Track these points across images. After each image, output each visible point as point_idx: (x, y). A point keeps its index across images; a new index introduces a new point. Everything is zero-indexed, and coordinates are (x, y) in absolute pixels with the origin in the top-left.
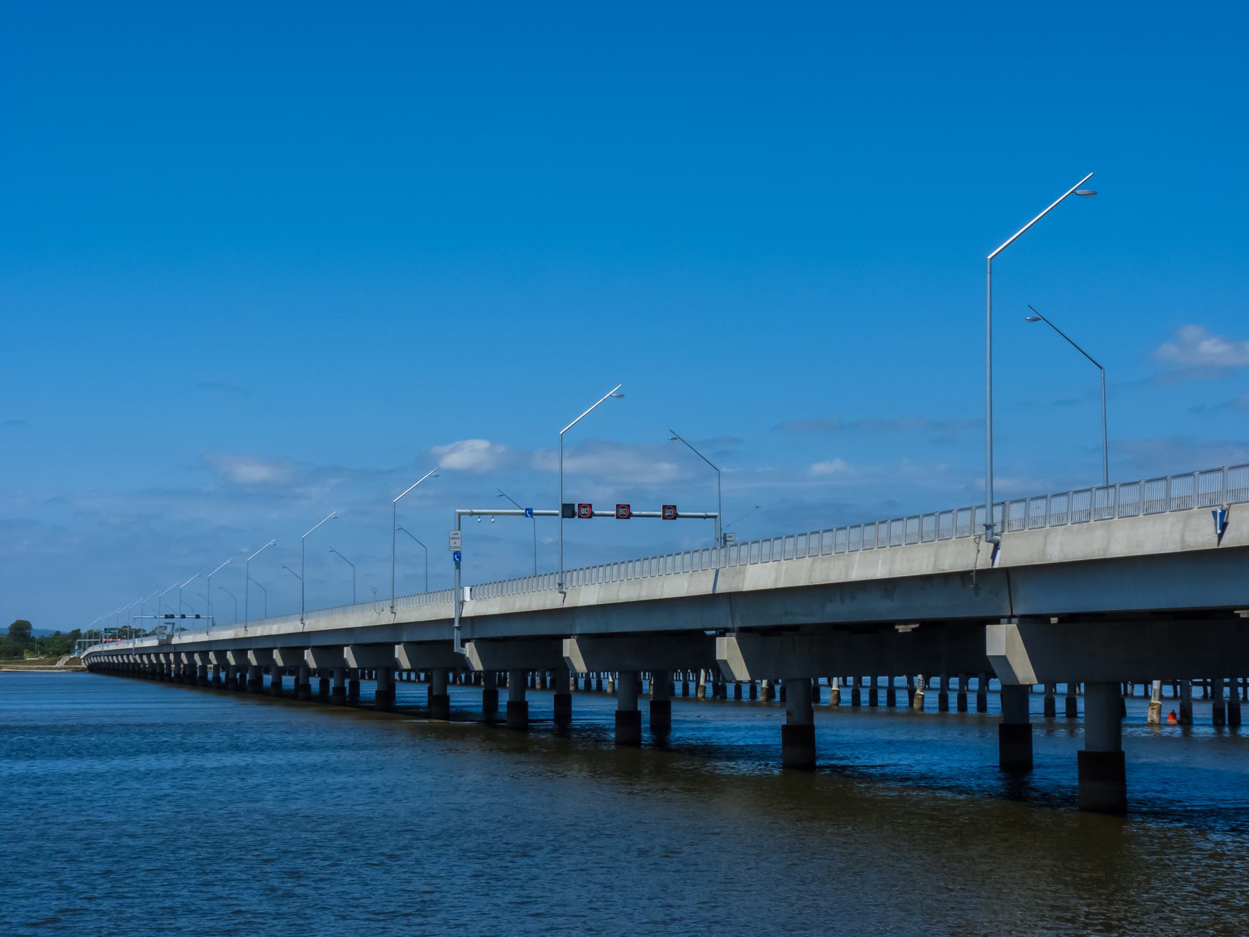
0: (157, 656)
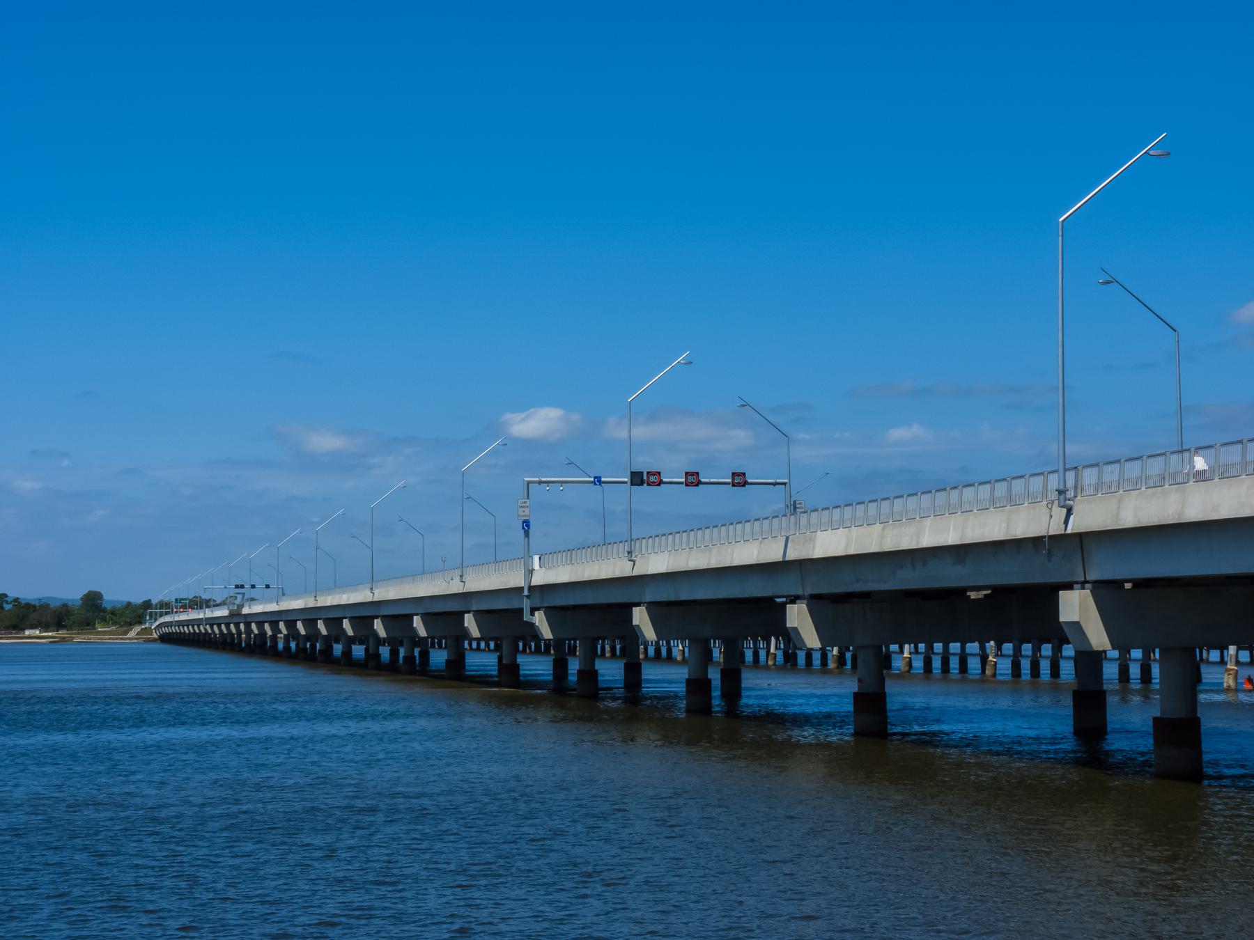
0: (228, 625)
